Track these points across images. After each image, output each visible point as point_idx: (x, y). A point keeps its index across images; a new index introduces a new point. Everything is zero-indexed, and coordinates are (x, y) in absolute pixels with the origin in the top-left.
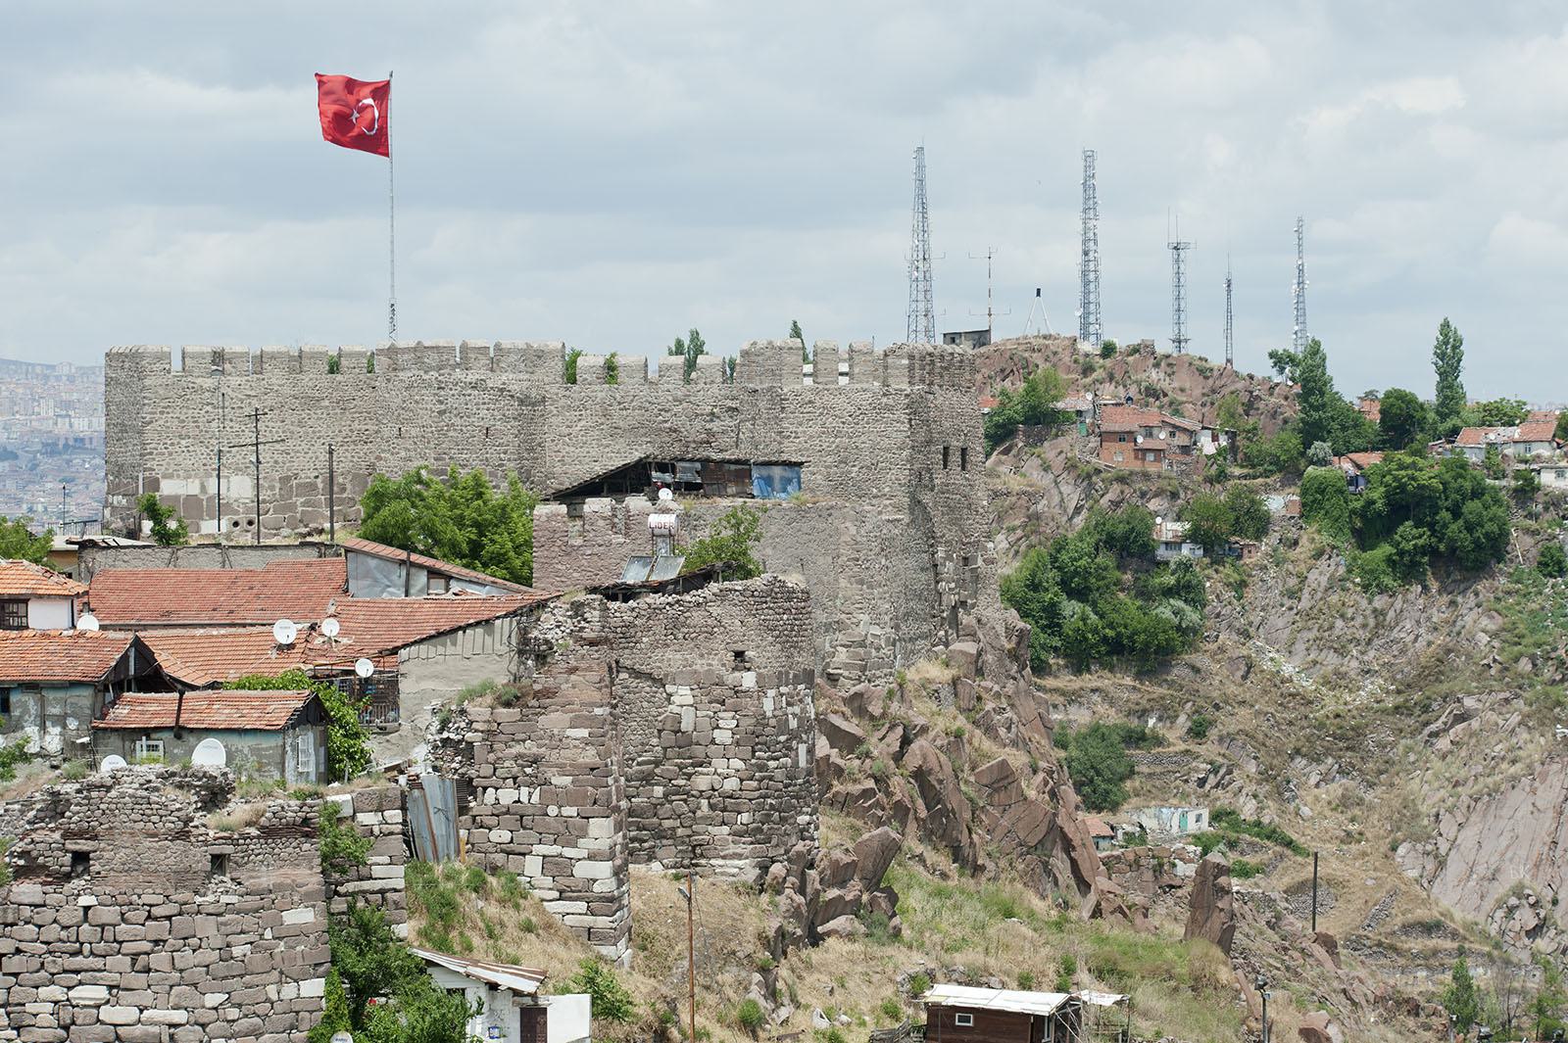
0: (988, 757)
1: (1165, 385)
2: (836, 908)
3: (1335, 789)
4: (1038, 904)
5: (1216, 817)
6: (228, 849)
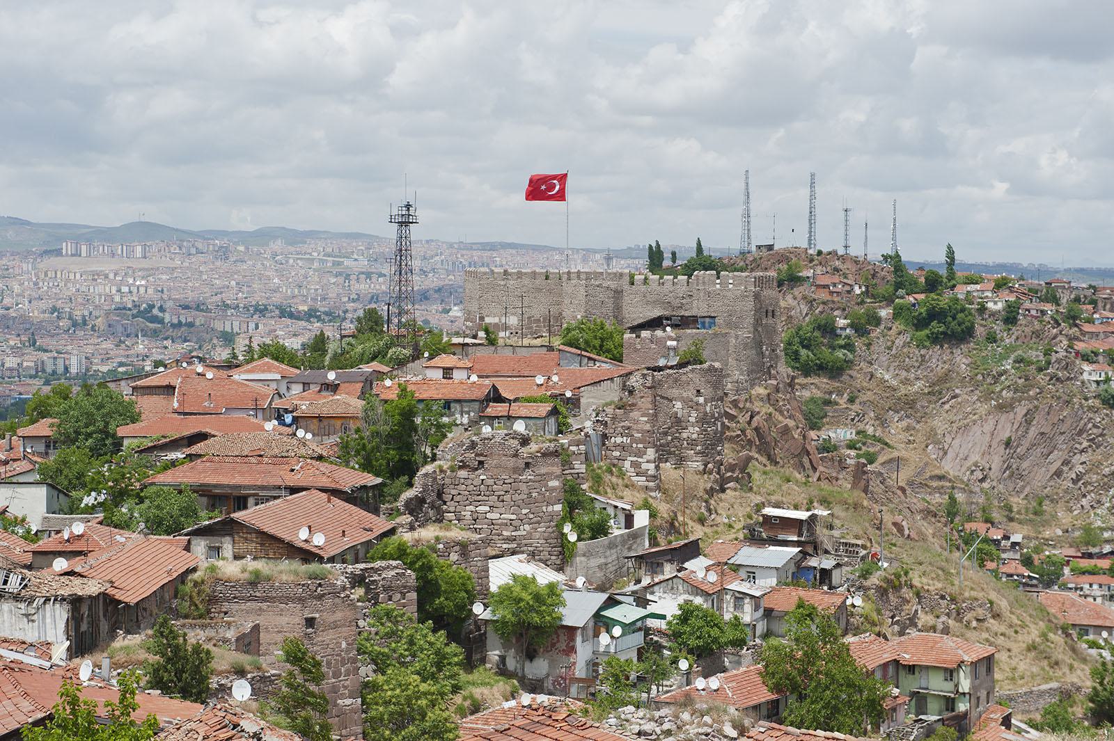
0: (781, 422)
1: (841, 267)
2: (730, 479)
3: (904, 424)
4: (798, 476)
5: (858, 433)
6: (531, 460)
